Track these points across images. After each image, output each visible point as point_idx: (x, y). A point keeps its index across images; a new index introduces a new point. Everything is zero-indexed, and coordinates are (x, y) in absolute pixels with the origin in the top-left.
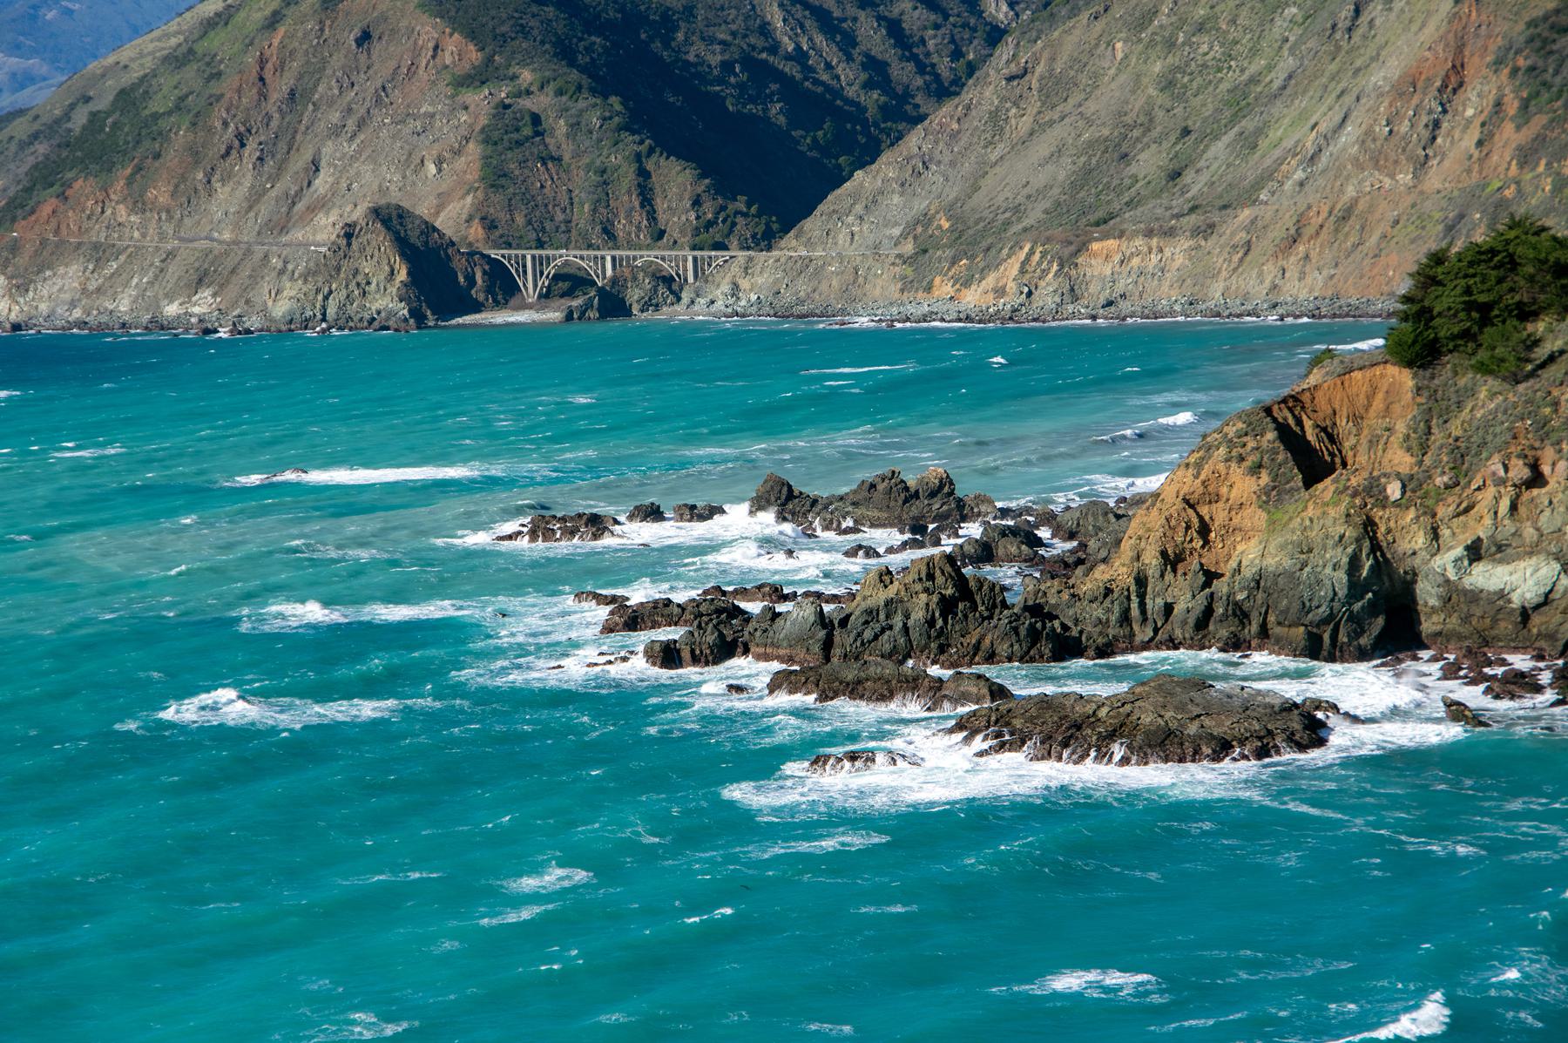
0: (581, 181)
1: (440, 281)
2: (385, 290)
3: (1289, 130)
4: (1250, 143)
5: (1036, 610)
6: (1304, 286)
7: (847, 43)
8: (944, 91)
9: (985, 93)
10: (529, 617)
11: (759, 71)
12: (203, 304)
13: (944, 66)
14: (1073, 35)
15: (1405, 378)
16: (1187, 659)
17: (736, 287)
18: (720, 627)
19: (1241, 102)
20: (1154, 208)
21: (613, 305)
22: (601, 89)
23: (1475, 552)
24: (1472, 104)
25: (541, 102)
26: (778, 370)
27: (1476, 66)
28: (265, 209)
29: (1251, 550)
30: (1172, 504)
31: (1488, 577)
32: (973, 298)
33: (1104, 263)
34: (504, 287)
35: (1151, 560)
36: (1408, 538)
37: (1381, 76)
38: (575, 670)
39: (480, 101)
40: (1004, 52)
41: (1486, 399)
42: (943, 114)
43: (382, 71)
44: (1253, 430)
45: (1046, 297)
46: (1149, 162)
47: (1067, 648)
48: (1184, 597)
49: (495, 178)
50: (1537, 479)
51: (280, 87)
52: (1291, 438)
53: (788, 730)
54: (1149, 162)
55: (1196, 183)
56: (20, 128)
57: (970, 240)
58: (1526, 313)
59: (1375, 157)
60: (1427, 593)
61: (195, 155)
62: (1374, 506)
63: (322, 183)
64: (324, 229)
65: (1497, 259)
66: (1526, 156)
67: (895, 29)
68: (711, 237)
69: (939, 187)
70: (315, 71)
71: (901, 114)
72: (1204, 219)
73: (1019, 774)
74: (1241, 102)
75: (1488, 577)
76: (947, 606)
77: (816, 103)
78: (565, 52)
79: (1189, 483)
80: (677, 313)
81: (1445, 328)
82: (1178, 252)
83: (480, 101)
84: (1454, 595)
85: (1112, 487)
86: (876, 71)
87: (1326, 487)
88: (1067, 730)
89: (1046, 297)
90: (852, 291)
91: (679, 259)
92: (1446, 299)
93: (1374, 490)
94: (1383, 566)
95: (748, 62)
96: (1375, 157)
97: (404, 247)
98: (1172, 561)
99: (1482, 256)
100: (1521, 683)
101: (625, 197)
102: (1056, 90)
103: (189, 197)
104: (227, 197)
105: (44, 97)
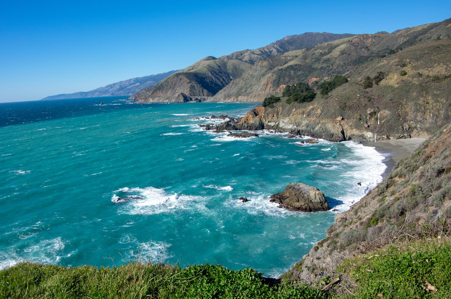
0: (198, 91)
1: (186, 99)
2: (182, 100)
3: (255, 88)
4: (252, 89)
5: (234, 126)
6: (256, 100)
7: (219, 80)
8: (227, 84)
9: (230, 84)
10: (193, 126)
11: (212, 82)
12: (167, 101)
13: (227, 82)
14: (237, 80)
15: (264, 108)
16: (246, 130)
17: (210, 99)
18: (208, 128)
19: (251, 85)
20: (244, 94)
21: (200, 101)
22: (199, 84)
23: (269, 122)
24: (269, 86)
25: (194, 85)
26: (213, 106)
27: (269, 83)
28: (172, 93)
29: (251, 121)
30: (245, 118)
31: (270, 124)
32: (229, 101)
33: (240, 98)
34: (191, 99)
35: (243, 122)
36: (264, 121)
37: (262, 84)
38: (196, 130)
39: (190, 85)
40: (232, 81)
41: (270, 110)
42: (227, 86)
43: (182, 82)
44: (252, 112)
45: (235, 101)
46: (243, 90)
47: (237, 129)
48: (246, 125)
49: (191, 91)
50: (274, 116)
51: (174, 84)
52: (255, 112)
53: (214, 135)
54: (243, 90)
55: (247, 92)
56: (153, 87)
57: (229, 96)
58: (273, 103)
59: (261, 90)
60: (265, 125)
61: (167, 89)
62: (230, 288)
63: (177, 91)
64: (177, 95)
65: (271, 99)
66: (273, 91)
67: (223, 79)
68: (208, 96)
69: (227, 92)
70: (176, 82)
71: (224, 86)
72: (248, 95)
73: (232, 139)
74: (251, 85)
75: (270, 124)
76: (227, 126)
77: (216, 85)
78: (196, 81)
79: (246, 116)
80: (205, 102)
81: (267, 104)
82: (246, 97)
83: (190, 85)
84: (267, 125)
85: (241, 116)
86: (222, 82)
87: (257, 116)
88: (237, 135)
89: (235, 101)
90: (219, 100)
91: (206, 97)
92: (267, 102)
93: (261, 117)
94: (262, 123)
95: (211, 82)
96: (261, 90)
97: (183, 96)
98: (245, 122)
99: (270, 98)
100: (272, 132)
101: (201, 92)
102: (236, 84)
103: (166, 92)
104: (169, 92)
105: (155, 85)
